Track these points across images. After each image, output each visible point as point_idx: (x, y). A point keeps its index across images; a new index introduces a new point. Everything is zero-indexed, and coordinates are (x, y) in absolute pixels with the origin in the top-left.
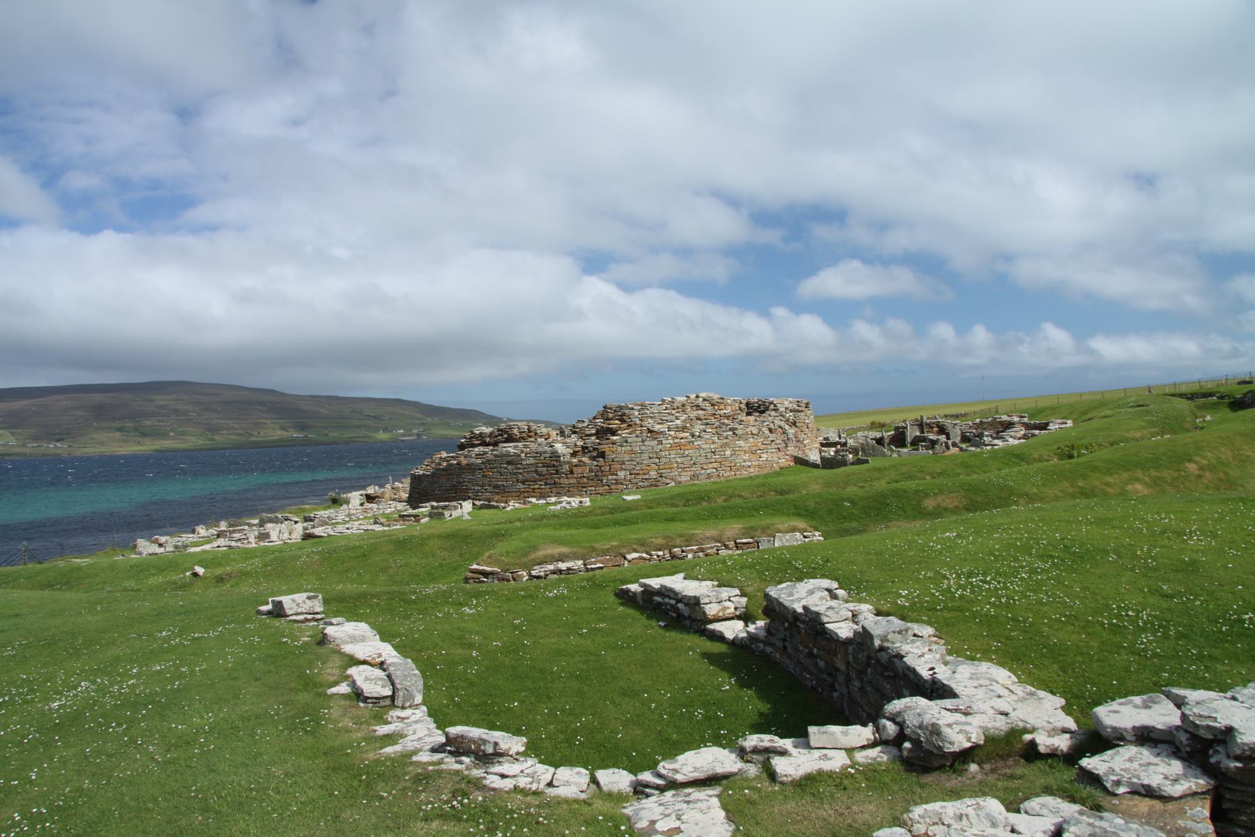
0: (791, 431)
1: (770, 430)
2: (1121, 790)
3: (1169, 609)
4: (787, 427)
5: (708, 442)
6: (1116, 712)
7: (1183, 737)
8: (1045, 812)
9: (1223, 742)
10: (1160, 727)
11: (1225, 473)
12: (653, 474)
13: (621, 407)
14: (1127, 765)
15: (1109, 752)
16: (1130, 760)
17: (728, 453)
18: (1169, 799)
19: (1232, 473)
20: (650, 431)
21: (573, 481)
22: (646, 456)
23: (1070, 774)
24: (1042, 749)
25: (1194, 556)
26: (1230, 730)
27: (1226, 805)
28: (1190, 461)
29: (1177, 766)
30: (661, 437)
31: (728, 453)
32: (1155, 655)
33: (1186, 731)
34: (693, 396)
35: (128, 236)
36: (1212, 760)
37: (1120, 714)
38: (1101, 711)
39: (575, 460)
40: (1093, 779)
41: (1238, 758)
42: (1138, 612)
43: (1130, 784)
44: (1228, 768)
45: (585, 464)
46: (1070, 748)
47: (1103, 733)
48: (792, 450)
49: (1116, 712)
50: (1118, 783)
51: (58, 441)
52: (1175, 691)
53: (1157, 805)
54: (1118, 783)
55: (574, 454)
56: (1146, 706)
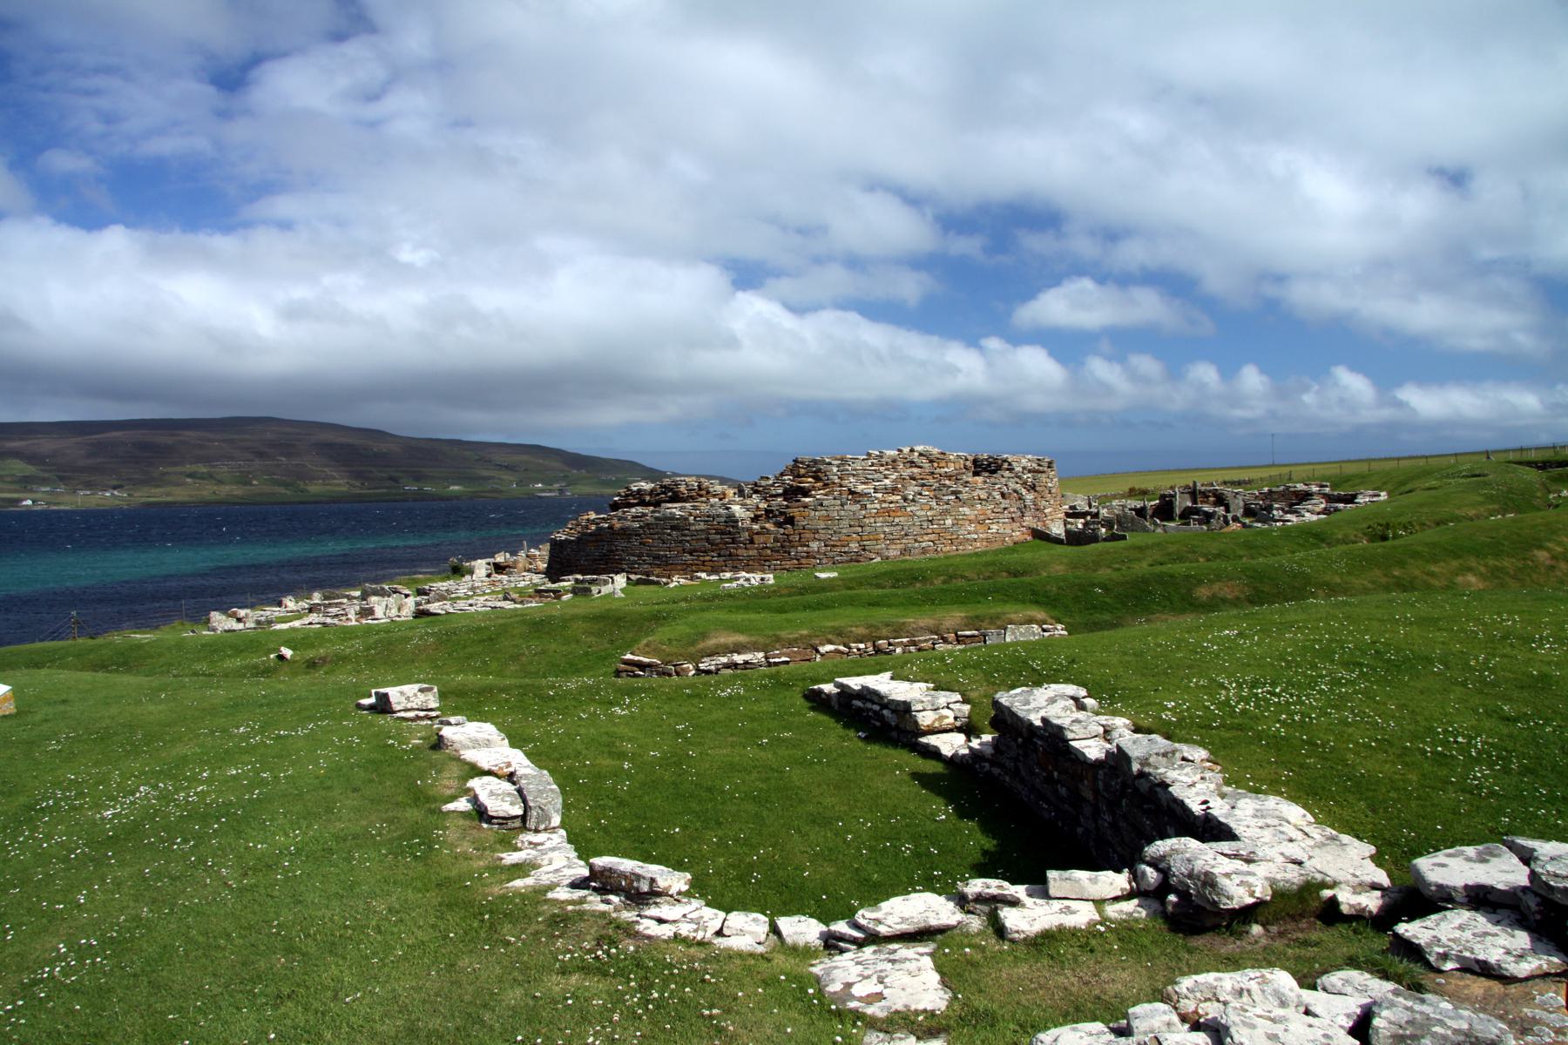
0: (1029, 497)
1: (1003, 495)
2: (1449, 966)
3: (1510, 736)
4: (1024, 492)
5: (927, 506)
6: (1443, 865)
8: (1349, 989)
10: (1500, 887)
12: (854, 546)
13: (815, 462)
14: (1457, 934)
16: (1461, 928)
17: (949, 522)
20: (851, 492)
21: (754, 552)
22: (845, 523)
23: (1383, 942)
24: (1345, 909)
25: (1545, 669)
28: (1540, 547)
29: (1522, 939)
30: (865, 501)
31: (949, 522)
32: (1492, 793)
33: (1536, 894)
34: (906, 450)
38: (1423, 863)
39: (756, 527)
40: (1413, 951)
42: (1470, 738)
43: (1459, 958)
45: (769, 532)
46: (1381, 908)
48: (1029, 521)
49: (1443, 865)
50: (1445, 957)
51: (115, 488)
52: (1521, 841)
53: (1497, 987)
54: (1445, 957)
55: (755, 519)
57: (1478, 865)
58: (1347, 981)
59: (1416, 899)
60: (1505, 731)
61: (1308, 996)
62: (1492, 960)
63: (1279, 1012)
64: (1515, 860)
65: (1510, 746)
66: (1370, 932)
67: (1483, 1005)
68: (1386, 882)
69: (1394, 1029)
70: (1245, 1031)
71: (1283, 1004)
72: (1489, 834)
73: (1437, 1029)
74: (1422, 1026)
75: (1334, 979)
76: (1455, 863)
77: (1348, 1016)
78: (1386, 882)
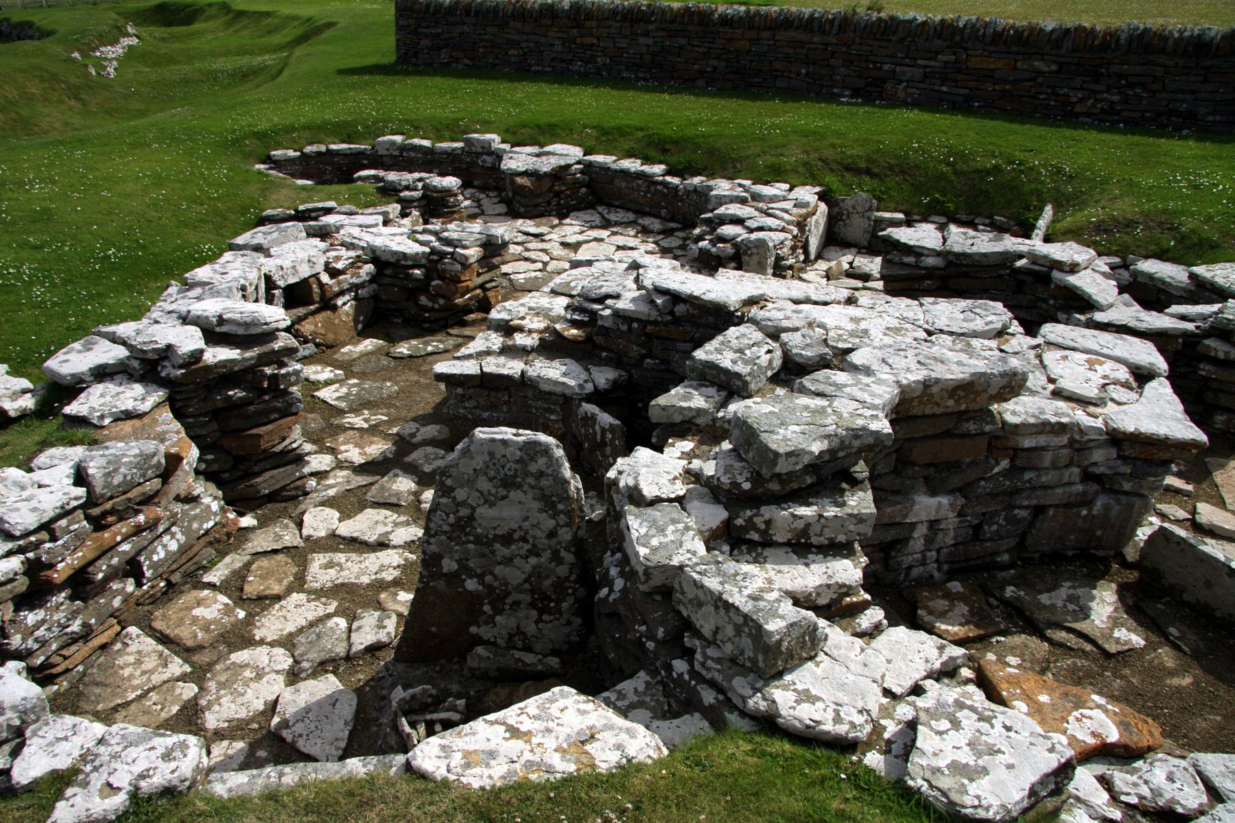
2: (107, 421)
3: (44, 259)
6: (67, 361)
7: (136, 364)
8: (56, 462)
9: (166, 358)
10: (111, 362)
11: (17, 113)
14: (102, 400)
15: (82, 395)
16: (102, 396)
18: (145, 414)
19: (23, 113)
23: (52, 424)
24: (12, 414)
25: (43, 204)
26: (169, 347)
27: (179, 405)
29: (138, 389)
32: (55, 304)
33: (136, 358)
35: (394, 48)
36: (163, 374)
37: (71, 361)
38: (53, 364)
40: (82, 421)
41: (181, 367)
42: (18, 268)
43: (112, 414)
44: (176, 377)
46: (36, 404)
47: (64, 382)
49: (67, 361)
50: (102, 417)
52: (104, 329)
53: (136, 422)
54: (102, 417)
56: (88, 349)
57: (87, 354)
58: (51, 457)
59: (71, 388)
60: (39, 257)
61: (37, 476)
62: (130, 408)
63: (26, 494)
64: (108, 343)
65: (47, 266)
66: (36, 423)
67: (136, 435)
68: (31, 386)
69: (103, 471)
70: (14, 515)
71: (23, 488)
72: (81, 331)
73: (125, 460)
74: (116, 462)
75: (42, 459)
76: (72, 357)
77: (68, 476)
78: (31, 386)
